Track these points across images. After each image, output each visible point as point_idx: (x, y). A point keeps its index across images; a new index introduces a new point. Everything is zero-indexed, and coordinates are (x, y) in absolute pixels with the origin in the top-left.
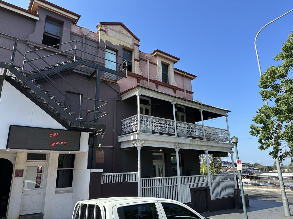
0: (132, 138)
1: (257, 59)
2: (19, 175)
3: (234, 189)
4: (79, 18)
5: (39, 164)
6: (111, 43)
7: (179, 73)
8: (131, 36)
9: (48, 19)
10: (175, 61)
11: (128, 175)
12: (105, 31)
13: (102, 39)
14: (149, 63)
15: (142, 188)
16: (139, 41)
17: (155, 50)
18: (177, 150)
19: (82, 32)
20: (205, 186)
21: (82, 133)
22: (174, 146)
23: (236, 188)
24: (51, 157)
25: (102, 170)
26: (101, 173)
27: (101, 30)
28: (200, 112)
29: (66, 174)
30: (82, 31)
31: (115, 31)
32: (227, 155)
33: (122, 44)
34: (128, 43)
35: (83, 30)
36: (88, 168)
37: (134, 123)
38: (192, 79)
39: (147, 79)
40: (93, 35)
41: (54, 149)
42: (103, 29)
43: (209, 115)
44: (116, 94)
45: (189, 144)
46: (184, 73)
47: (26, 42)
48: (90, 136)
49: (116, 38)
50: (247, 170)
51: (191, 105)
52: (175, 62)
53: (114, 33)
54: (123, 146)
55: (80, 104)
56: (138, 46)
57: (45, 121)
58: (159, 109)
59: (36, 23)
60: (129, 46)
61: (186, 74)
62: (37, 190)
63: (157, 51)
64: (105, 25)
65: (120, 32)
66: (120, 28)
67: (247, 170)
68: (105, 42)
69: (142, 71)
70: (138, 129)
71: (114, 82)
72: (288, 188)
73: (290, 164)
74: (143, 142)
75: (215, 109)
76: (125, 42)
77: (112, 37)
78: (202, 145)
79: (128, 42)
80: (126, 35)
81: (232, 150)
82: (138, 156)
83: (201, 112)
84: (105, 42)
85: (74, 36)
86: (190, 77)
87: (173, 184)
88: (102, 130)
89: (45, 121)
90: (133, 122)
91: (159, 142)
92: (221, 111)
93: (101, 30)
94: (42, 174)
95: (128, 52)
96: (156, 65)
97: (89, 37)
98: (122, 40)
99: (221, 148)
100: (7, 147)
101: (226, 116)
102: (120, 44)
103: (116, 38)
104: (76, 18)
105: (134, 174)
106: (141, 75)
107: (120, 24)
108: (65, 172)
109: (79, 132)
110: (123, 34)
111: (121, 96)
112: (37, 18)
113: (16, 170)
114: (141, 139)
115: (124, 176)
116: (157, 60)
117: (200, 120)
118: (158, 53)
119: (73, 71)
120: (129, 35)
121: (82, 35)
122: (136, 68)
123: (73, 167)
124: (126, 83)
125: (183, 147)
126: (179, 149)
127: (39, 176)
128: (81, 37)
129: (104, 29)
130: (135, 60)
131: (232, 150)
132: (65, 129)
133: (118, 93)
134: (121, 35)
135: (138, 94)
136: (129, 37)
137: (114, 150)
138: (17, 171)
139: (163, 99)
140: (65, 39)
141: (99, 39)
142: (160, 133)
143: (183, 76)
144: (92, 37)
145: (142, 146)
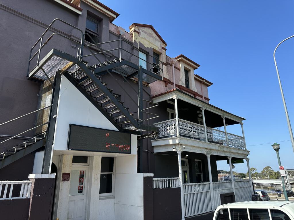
0: (171, 142)
1: (276, 71)
2: (66, 179)
3: (252, 195)
4: (117, 17)
5: (80, 167)
6: (143, 45)
7: (200, 80)
8: (159, 40)
9: (89, 14)
10: (196, 67)
11: (172, 180)
12: (138, 33)
13: (136, 41)
14: (174, 67)
15: (184, 193)
16: (166, 45)
17: (180, 55)
18: (209, 156)
19: (119, 32)
20: (230, 191)
21: (132, 135)
22: (206, 151)
23: (253, 194)
24: (94, 160)
25: (153, 174)
26: (152, 177)
27: (135, 31)
28: (222, 119)
29: (106, 178)
30: (119, 30)
31: (146, 33)
32: (242, 162)
33: (153, 47)
34: (157, 47)
35: (120, 30)
36: (139, 171)
37: (171, 127)
38: (208, 86)
39: (173, 83)
40: (128, 35)
41: (108, 151)
42: (136, 30)
43: (230, 122)
44: (148, 97)
45: (217, 150)
46: (203, 79)
47: (70, 36)
48: (138, 137)
49: (147, 40)
50: (228, 177)
51: (216, 111)
52: (195, 69)
53: (146, 35)
54: (156, 151)
55: (138, 105)
56: (165, 50)
57: (102, 122)
58: (189, 113)
59: (79, 18)
60: (158, 50)
61: (204, 81)
62: (80, 196)
63: (182, 56)
64: (138, 26)
65: (150, 35)
66: (150, 31)
67: (228, 177)
68: (138, 44)
69: (169, 75)
70: (178, 134)
71: (147, 84)
72: (275, 194)
73: (262, 172)
74: (184, 147)
75: (230, 115)
76: (154, 45)
77: (144, 39)
78: (226, 152)
79: (157, 45)
80: (155, 38)
81: (248, 157)
82: (179, 161)
83: (224, 119)
84: (138, 44)
85: (112, 34)
86: (206, 84)
87: (190, 192)
88: (155, 133)
89: (102, 122)
90: (169, 126)
91: (195, 148)
92: (235, 117)
93: (135, 31)
94: (84, 178)
95: (157, 55)
96: (179, 70)
97: (124, 37)
98: (152, 43)
99: (239, 155)
100: (69, 148)
101: (242, 124)
102: (151, 47)
103: (147, 40)
104: (115, 16)
105: (25, 184)
106: (169, 79)
107: (81, 31)
108: (104, 176)
109: (129, 134)
110: (152, 37)
111: (153, 99)
112: (80, 13)
113: (63, 174)
114: (182, 143)
115: (169, 181)
116: (180, 65)
117: (223, 125)
118: (183, 58)
119: (112, 71)
120: (157, 38)
121: (119, 34)
122: (164, 73)
123: (112, 171)
124: (157, 87)
125: (212, 153)
126: (211, 155)
127: (81, 181)
128: (117, 36)
129: (137, 30)
130: (163, 63)
131: (248, 157)
132: (118, 130)
133: (150, 96)
134: (152, 38)
135: (176, 98)
136: (158, 41)
137: (149, 153)
138: (63, 174)
139: (195, 104)
140: (105, 37)
141: (132, 40)
142: (195, 138)
143: (201, 82)
144: (127, 37)
145: (182, 151)
